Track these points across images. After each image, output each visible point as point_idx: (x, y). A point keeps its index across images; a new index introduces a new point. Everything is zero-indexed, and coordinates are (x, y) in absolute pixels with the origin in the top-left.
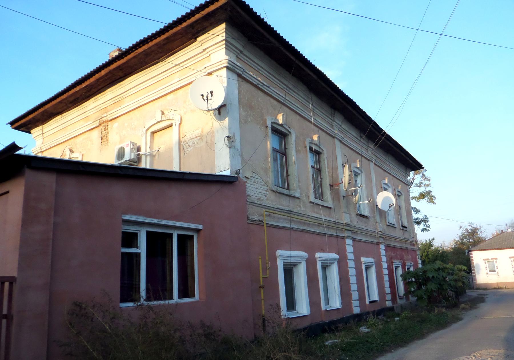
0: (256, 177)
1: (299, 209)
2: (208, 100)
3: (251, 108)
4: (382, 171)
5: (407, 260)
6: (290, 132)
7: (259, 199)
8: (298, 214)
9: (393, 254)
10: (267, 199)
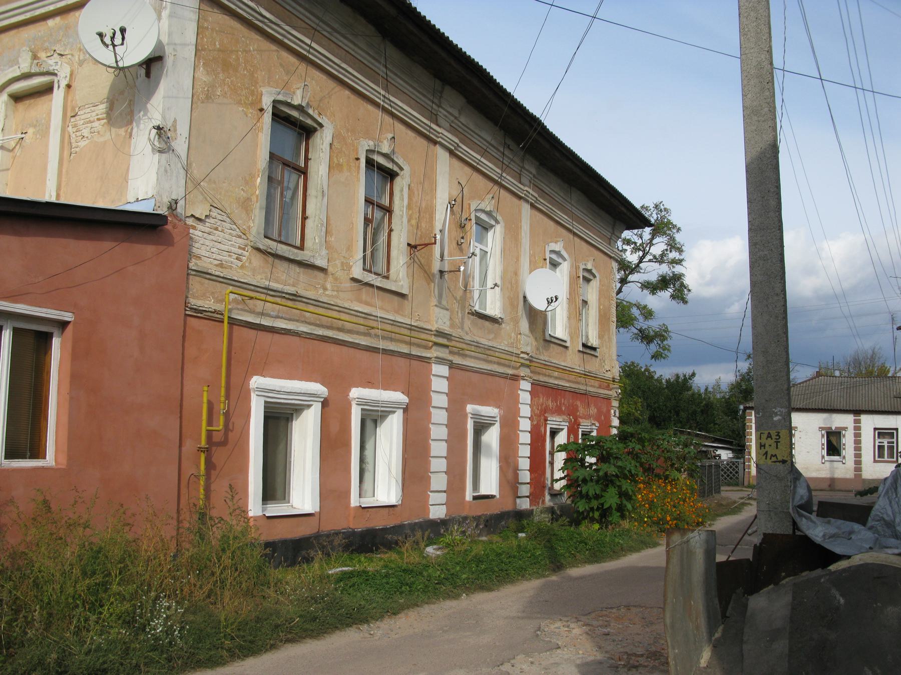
0: (219, 217)
1: (321, 291)
2: (114, 46)
3: (227, 66)
4: (552, 223)
5: (587, 417)
6: (321, 126)
7: (221, 265)
8: (317, 303)
9: (550, 403)
10: (242, 267)
